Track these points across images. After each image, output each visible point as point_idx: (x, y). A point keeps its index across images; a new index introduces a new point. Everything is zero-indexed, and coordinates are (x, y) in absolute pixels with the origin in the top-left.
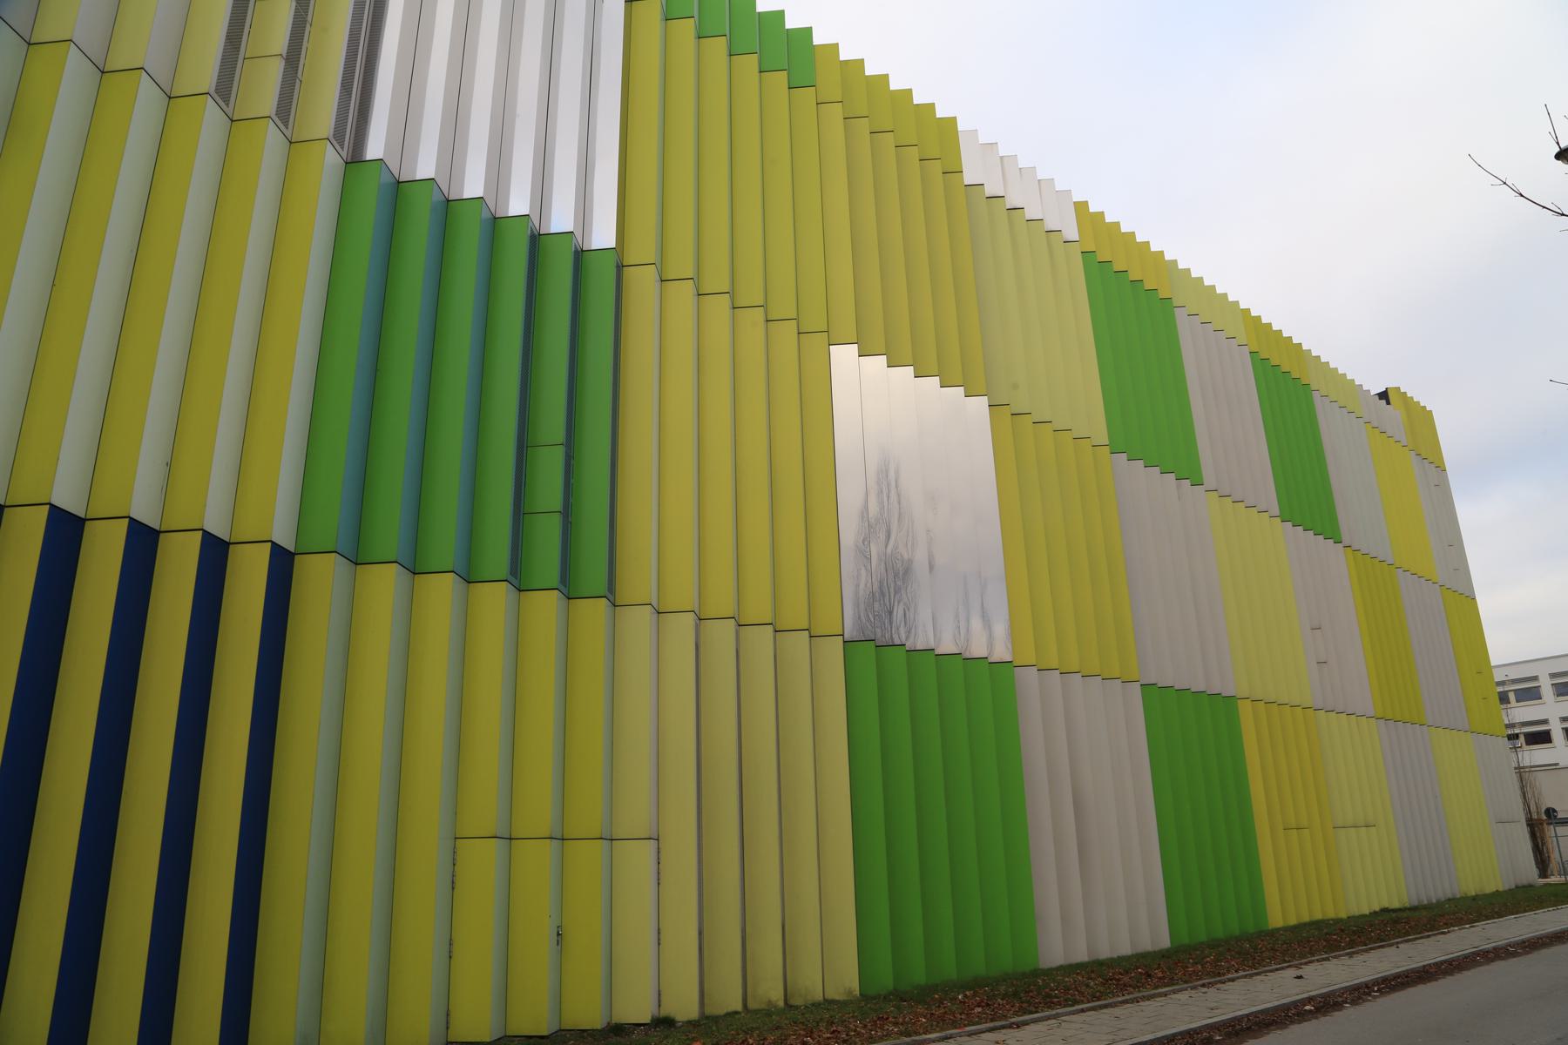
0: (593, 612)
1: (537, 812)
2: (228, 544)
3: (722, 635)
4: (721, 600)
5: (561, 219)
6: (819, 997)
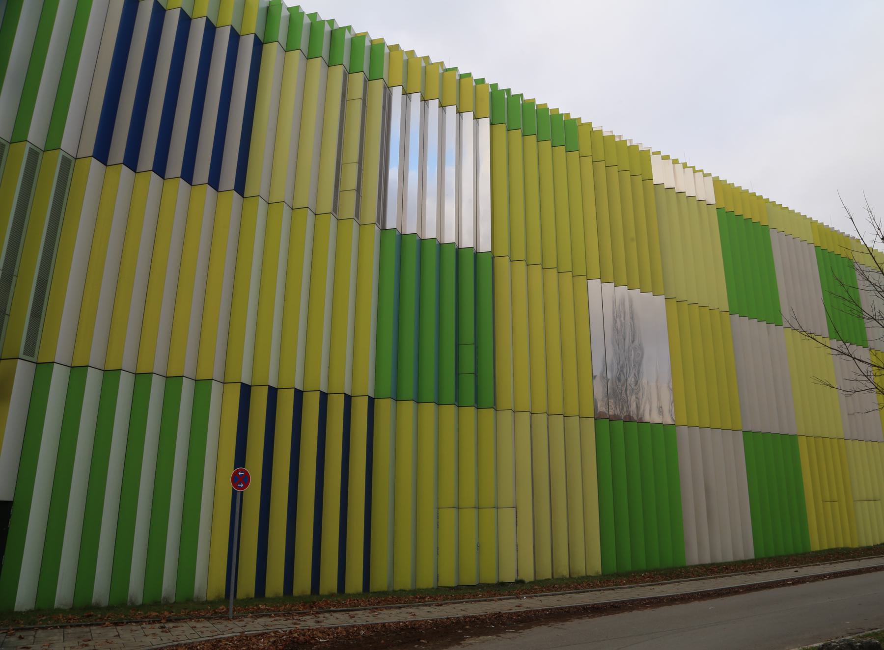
0: (488, 414)
1: (469, 498)
2: (276, 389)
3: (541, 420)
4: (541, 405)
5: (467, 242)
6: (584, 574)
